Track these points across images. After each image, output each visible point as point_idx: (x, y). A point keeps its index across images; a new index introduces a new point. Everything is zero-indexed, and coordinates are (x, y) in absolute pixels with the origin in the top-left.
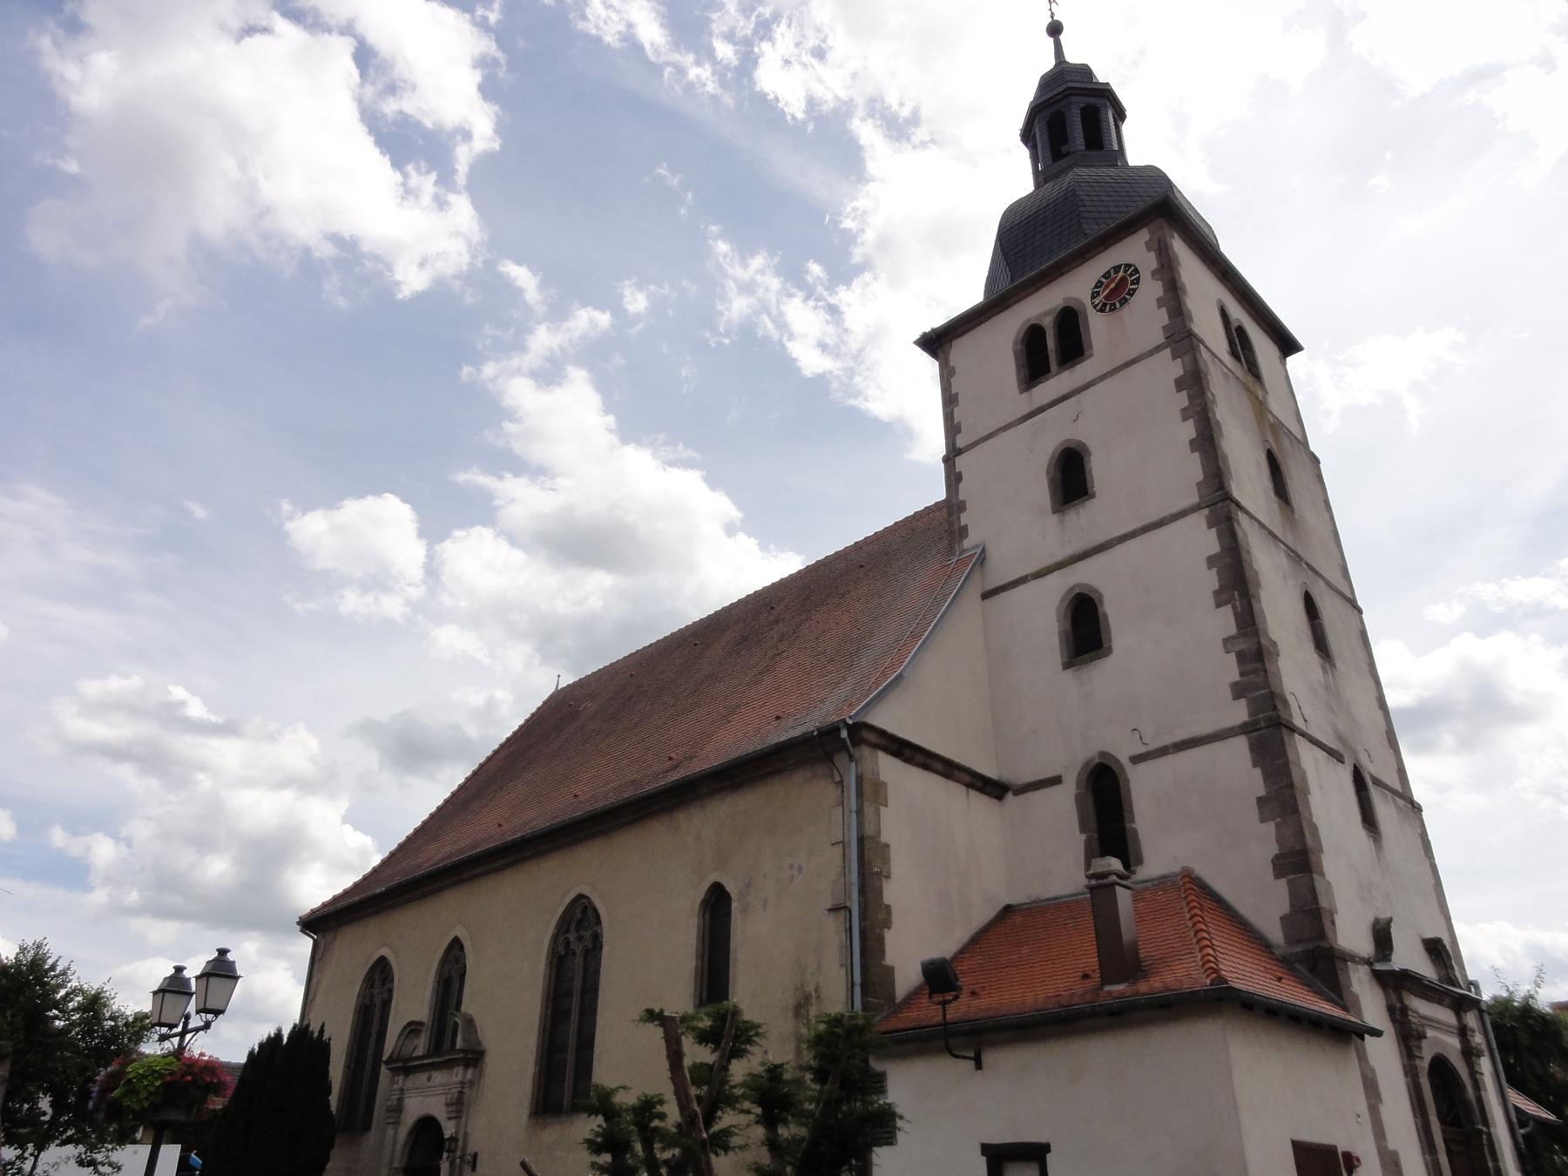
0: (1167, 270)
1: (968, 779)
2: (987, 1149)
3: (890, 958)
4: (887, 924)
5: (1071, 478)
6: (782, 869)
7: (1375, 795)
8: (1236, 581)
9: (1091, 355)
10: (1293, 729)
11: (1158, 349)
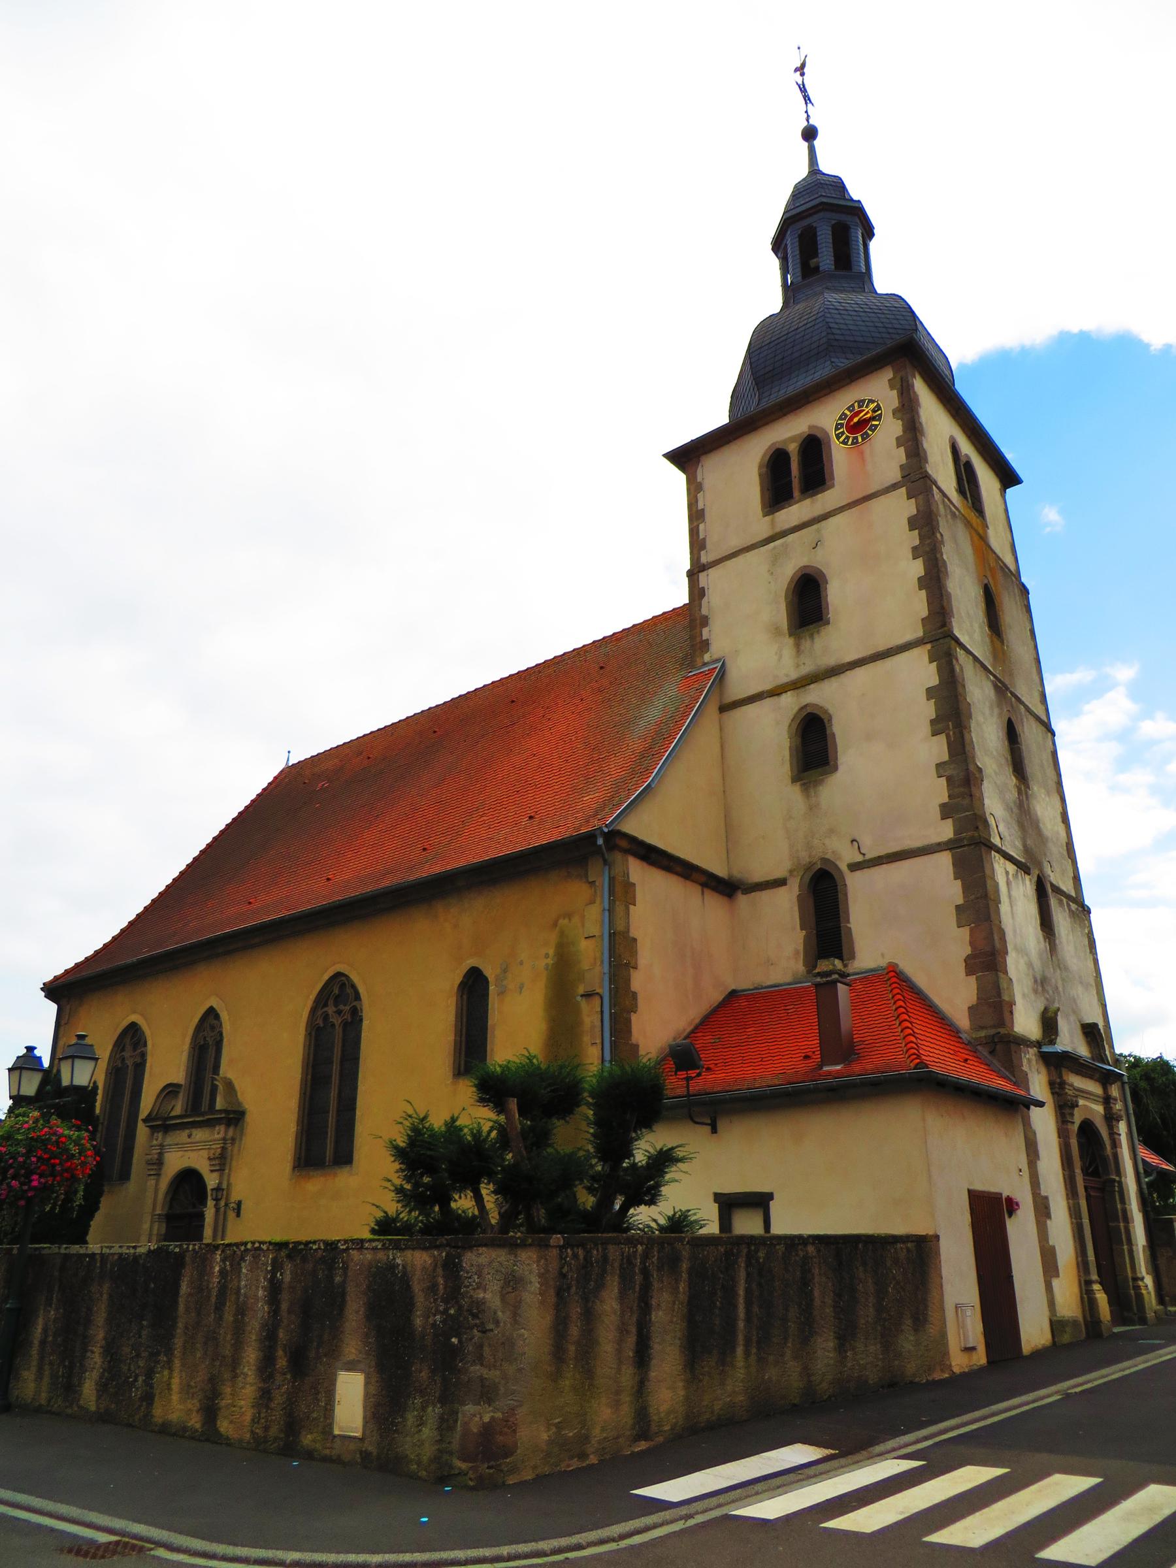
0: (908, 410)
1: (703, 879)
2: (718, 1197)
3: (637, 1036)
4: (634, 1009)
5: (807, 602)
6: (522, 951)
7: (1053, 902)
8: (951, 714)
9: (833, 486)
10: (992, 847)
11: (894, 487)
